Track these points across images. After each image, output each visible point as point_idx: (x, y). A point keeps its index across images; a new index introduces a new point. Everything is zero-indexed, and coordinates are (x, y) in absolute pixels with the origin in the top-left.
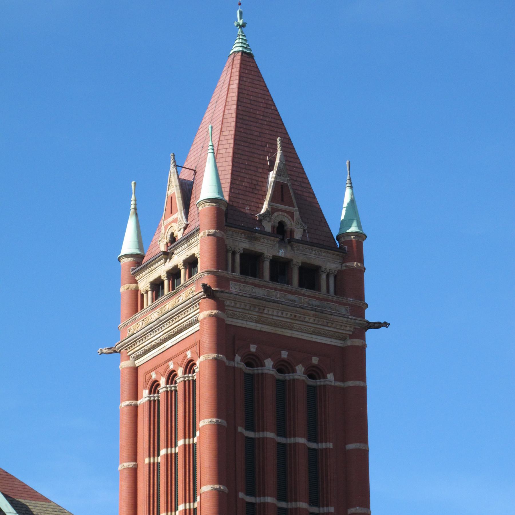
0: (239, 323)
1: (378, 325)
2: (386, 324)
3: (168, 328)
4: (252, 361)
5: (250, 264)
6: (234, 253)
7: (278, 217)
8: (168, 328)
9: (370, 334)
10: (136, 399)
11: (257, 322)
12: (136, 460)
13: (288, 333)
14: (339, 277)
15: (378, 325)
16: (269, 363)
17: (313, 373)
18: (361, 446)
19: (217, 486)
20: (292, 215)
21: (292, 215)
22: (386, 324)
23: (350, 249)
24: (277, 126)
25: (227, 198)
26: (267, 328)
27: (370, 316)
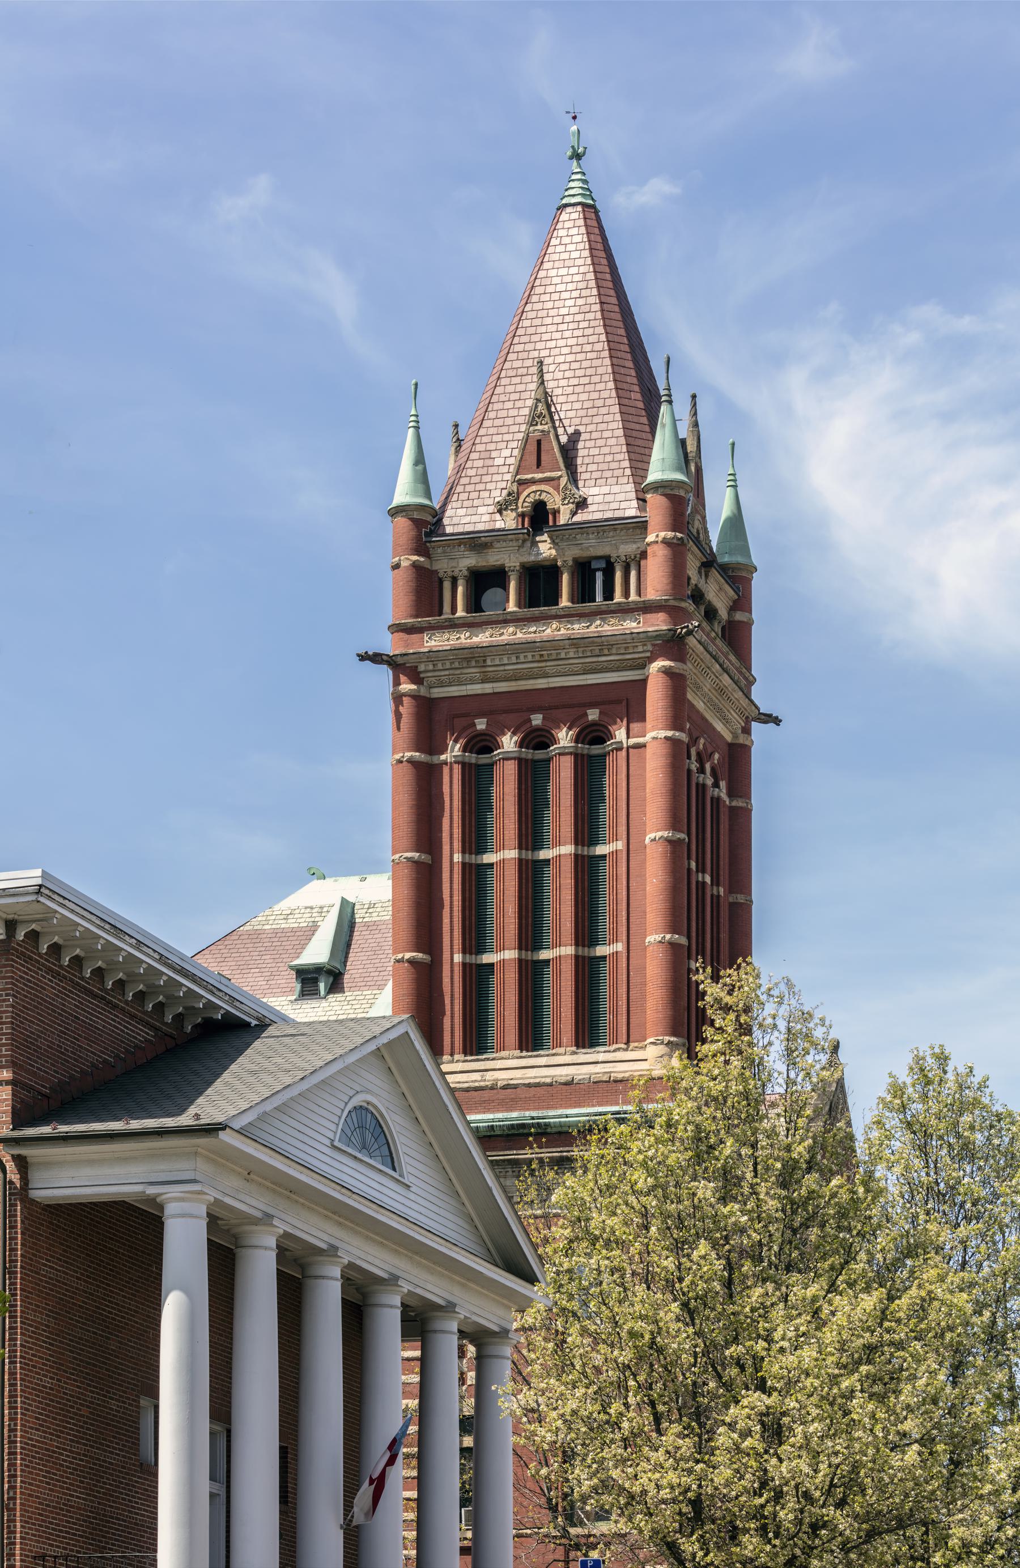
0: (454, 691)
6: (454, 581)
11: (483, 681)
13: (541, 683)
15: (376, 658)
26: (503, 687)
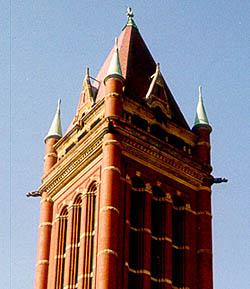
1: (219, 181)
2: (226, 181)
3: (86, 176)
4: (139, 183)
5: (138, 122)
7: (155, 104)
8: (86, 176)
9: (214, 186)
10: (51, 222)
12: (48, 259)
14: (195, 149)
15: (219, 181)
16: (168, 196)
17: (179, 201)
18: (207, 250)
19: (109, 251)
20: (165, 106)
21: (165, 106)
22: (226, 181)
23: (203, 132)
24: (151, 66)
25: (124, 76)
27: (214, 174)
